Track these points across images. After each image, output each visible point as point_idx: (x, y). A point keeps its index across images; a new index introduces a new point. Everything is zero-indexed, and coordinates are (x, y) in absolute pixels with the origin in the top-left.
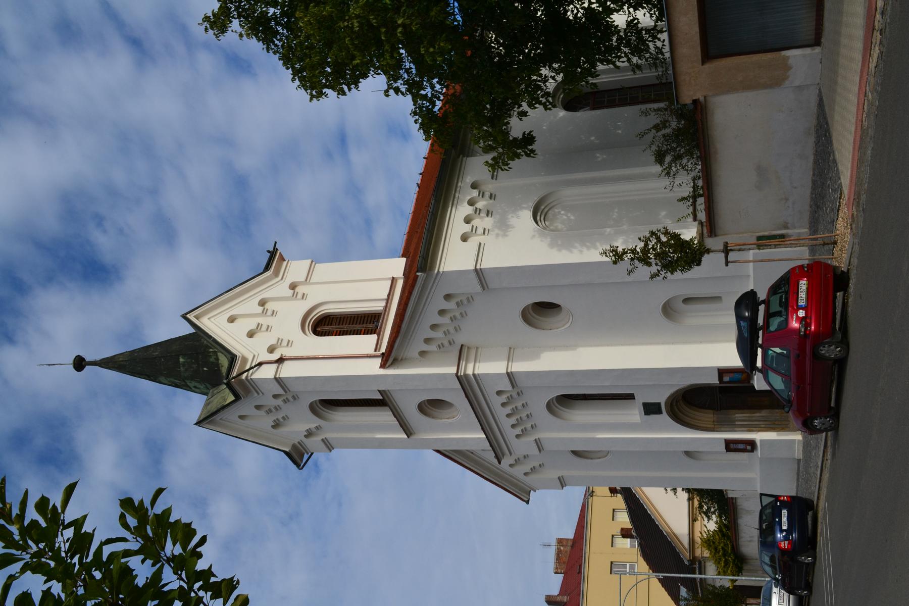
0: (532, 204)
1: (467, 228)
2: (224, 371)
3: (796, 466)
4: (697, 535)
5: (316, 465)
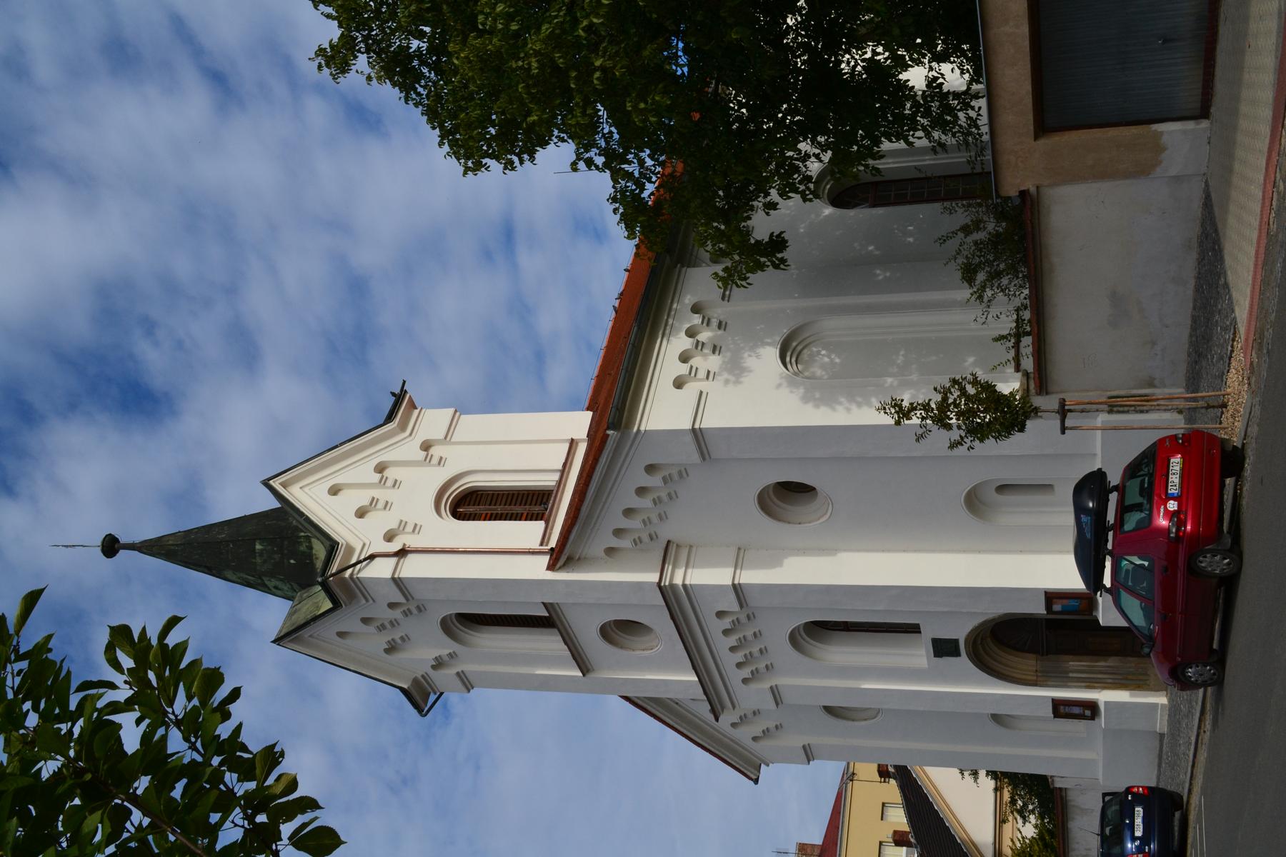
0: (779, 339)
1: (683, 369)
2: (319, 565)
3: (1157, 744)
4: (1007, 843)
5: (445, 706)
